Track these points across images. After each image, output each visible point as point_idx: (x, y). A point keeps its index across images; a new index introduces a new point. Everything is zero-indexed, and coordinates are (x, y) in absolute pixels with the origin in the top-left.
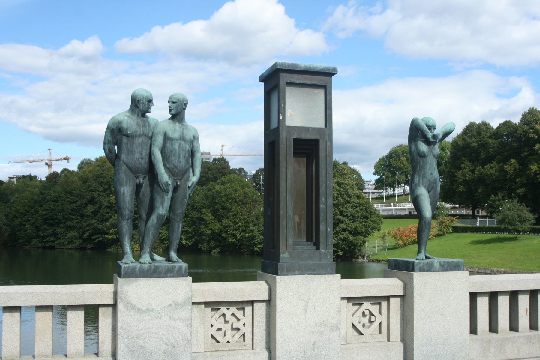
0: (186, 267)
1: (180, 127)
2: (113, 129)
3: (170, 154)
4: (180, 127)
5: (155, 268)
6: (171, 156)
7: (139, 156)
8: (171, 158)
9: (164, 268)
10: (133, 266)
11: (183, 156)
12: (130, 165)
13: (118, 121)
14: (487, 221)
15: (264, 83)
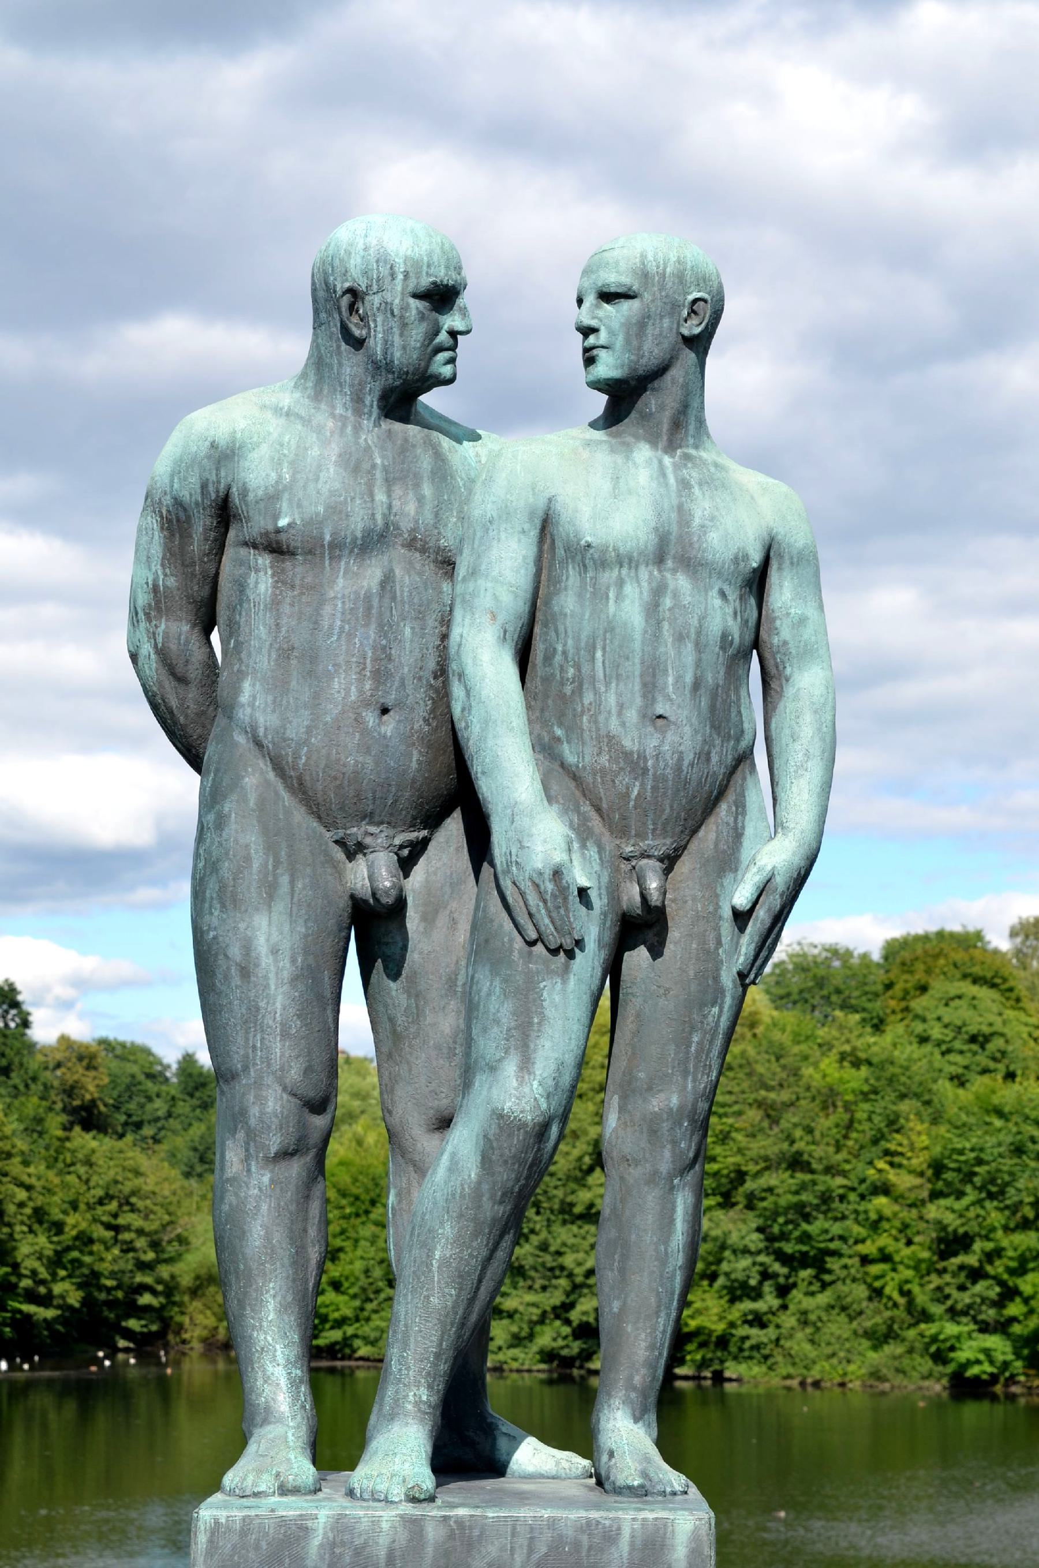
0: (695, 1537)
1: (663, 473)
3: (586, 669)
4: (663, 473)
6: (593, 679)
7: (361, 692)
8: (588, 698)
9: (522, 1541)
10: (283, 1521)
11: (679, 679)
13: (213, 445)
15: (606, 397)
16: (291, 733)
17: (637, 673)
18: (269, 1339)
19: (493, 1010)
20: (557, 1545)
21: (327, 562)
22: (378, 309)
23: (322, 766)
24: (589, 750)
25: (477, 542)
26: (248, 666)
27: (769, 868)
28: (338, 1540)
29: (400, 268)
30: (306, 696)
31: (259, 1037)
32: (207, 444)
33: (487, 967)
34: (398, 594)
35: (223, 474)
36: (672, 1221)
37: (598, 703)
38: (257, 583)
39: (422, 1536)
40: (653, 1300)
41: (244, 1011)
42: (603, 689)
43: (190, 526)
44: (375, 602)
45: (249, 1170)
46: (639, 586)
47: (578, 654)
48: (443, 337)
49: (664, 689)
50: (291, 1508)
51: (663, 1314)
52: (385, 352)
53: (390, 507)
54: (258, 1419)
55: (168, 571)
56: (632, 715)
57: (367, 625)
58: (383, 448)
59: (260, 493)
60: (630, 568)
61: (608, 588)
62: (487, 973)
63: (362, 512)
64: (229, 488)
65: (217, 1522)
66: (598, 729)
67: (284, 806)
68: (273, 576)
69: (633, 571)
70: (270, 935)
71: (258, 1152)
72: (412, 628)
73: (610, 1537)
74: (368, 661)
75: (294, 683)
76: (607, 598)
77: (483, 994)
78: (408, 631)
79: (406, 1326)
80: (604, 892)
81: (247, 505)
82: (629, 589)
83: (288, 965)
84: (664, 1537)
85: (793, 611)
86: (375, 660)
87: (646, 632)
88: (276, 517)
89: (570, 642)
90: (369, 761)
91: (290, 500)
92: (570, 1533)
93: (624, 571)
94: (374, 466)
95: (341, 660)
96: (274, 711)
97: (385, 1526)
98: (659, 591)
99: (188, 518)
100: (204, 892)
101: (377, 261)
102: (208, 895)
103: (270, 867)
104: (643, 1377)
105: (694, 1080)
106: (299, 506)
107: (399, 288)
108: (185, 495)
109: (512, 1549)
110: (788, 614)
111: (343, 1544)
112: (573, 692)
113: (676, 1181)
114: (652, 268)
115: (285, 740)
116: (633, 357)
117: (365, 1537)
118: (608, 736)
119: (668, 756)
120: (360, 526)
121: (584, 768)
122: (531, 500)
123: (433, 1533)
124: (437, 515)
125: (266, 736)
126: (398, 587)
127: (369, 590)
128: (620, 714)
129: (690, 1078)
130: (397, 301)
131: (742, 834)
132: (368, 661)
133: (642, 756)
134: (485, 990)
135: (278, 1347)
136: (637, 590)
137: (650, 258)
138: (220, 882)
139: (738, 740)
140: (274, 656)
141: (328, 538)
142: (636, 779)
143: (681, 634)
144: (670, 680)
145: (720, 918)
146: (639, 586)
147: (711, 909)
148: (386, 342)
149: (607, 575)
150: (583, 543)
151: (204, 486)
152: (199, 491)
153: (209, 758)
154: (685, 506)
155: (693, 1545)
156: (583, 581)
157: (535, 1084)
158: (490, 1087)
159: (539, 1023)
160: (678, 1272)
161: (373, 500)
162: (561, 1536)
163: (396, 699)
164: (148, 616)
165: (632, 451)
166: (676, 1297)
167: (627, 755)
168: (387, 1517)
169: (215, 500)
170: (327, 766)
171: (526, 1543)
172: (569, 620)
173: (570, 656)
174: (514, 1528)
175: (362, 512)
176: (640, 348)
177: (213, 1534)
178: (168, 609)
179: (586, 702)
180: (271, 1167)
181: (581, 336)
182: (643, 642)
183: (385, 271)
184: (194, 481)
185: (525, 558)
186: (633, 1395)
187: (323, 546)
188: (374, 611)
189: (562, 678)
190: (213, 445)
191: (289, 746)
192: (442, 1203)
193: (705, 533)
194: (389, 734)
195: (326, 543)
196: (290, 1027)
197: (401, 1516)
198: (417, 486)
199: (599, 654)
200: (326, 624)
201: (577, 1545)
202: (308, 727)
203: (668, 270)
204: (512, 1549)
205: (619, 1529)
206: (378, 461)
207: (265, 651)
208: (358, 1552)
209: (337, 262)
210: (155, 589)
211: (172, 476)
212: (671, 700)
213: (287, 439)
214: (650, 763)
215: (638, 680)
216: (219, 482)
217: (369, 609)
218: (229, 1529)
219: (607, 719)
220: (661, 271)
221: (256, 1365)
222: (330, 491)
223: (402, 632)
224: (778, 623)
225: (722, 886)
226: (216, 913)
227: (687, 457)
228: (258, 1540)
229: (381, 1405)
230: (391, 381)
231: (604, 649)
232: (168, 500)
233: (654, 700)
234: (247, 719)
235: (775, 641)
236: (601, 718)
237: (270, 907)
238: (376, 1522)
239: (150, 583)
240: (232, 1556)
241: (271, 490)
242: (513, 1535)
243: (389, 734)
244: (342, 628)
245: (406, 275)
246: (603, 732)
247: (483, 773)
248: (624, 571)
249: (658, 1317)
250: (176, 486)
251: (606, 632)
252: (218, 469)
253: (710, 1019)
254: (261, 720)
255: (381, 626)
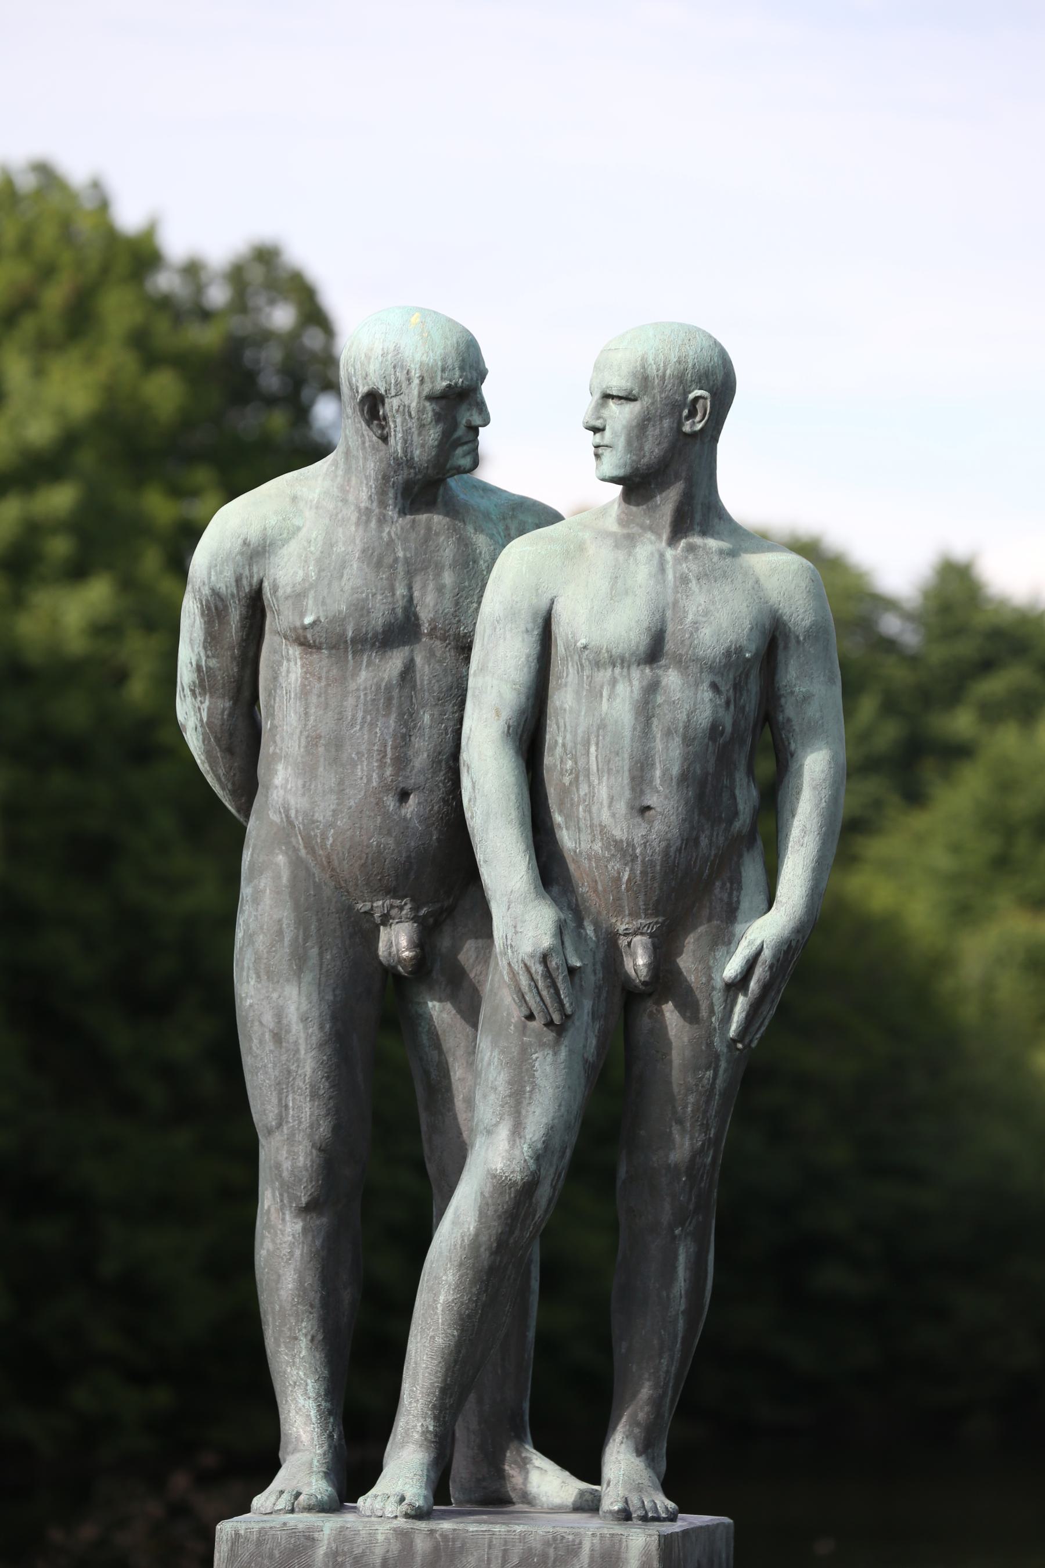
0: (646, 1552)
1: (662, 569)
2: (215, 593)
3: (581, 763)
4: (662, 569)
5: (436, 1549)
6: (588, 771)
7: (381, 777)
8: (584, 789)
9: (497, 1553)
10: (293, 1533)
11: (664, 773)
12: (324, 838)
13: (246, 543)
14: (450, 1504)
15: (621, 486)
16: (318, 816)
17: (626, 768)
18: (301, 1373)
19: (491, 1078)
20: (528, 1555)
21: (350, 657)
22: (397, 411)
23: (347, 846)
24: (585, 837)
25: (486, 639)
26: (281, 749)
27: (758, 942)
28: (340, 1549)
29: (415, 375)
30: (332, 781)
31: (290, 1097)
32: (240, 541)
33: (490, 1038)
34: (418, 683)
35: (255, 569)
36: (674, 1268)
37: (591, 794)
38: (288, 672)
39: (411, 1547)
40: (655, 1342)
41: (277, 1074)
42: (596, 782)
43: (227, 614)
44: (395, 693)
45: (283, 1220)
46: (631, 685)
47: (575, 747)
48: (461, 431)
49: (651, 782)
50: (303, 1520)
51: (666, 1355)
52: (405, 452)
53: (411, 599)
54: (290, 1448)
55: (209, 653)
56: (621, 807)
57: (387, 715)
58: (405, 540)
59: (289, 590)
60: (622, 668)
61: (602, 687)
62: (489, 1044)
63: (383, 607)
64: (261, 582)
65: (237, 1534)
66: (591, 819)
67: (315, 882)
68: (302, 666)
69: (625, 670)
70: (300, 1003)
71: (290, 1202)
72: (432, 715)
73: (573, 1550)
74: (389, 749)
75: (321, 769)
76: (601, 695)
77: (485, 1063)
78: (427, 718)
79: (416, 1363)
80: (599, 967)
81: (277, 600)
82: (622, 688)
83: (317, 1032)
84: (619, 1552)
85: (797, 689)
86: (394, 748)
87: (634, 729)
88: (302, 615)
89: (569, 736)
90: (391, 841)
91: (315, 598)
92: (538, 1546)
93: (617, 670)
94: (396, 560)
95: (363, 748)
96: (303, 795)
97: (380, 1538)
98: (652, 688)
99: (226, 607)
100: (243, 961)
101: (394, 367)
102: (245, 965)
103: (300, 940)
104: (648, 1414)
105: (691, 1139)
106: (324, 603)
107: (416, 392)
108: (221, 587)
109: (489, 1560)
110: (792, 693)
111: (344, 1554)
112: (571, 783)
113: (677, 1232)
114: (652, 371)
115: (313, 822)
116: (634, 458)
117: (364, 1547)
118: (600, 825)
119: (655, 844)
120: (380, 622)
121: (581, 853)
122: (534, 601)
123: (421, 1545)
124: (457, 603)
125: (297, 817)
126: (418, 676)
127: (390, 681)
128: (610, 806)
129: (688, 1137)
130: (414, 405)
131: (737, 909)
132: (389, 749)
133: (631, 844)
134: (486, 1059)
135: (309, 1381)
136: (629, 689)
137: (651, 361)
138: (256, 954)
139: (730, 822)
140: (303, 743)
141: (350, 634)
142: (626, 864)
143: (669, 729)
144: (658, 773)
145: (713, 988)
146: (631, 685)
147: (704, 980)
148: (405, 441)
149: (601, 673)
150: (579, 644)
151: (238, 580)
152: (234, 584)
153: (250, 833)
154: (681, 604)
155: (644, 1559)
156: (581, 678)
157: (525, 1147)
158: (487, 1149)
159: (530, 1092)
160: (680, 1317)
161: (394, 595)
162: (530, 1549)
163: (415, 784)
164: (193, 692)
165: (634, 546)
166: (679, 1340)
167: (617, 843)
168: (383, 1531)
169: (250, 592)
170: (351, 847)
171: (500, 1554)
172: (567, 714)
173: (569, 749)
174: (491, 1541)
175: (383, 607)
176: (641, 448)
177: (233, 1544)
178: (211, 687)
179: (582, 793)
180: (303, 1215)
181: (592, 433)
182: (632, 740)
183: (401, 376)
184: (229, 574)
185: (528, 656)
186: (637, 1430)
187: (346, 641)
188: (395, 702)
189: (562, 769)
190: (246, 543)
191: (318, 827)
192: (446, 1253)
193: (697, 629)
194: (409, 816)
195: (349, 638)
196: (319, 1088)
197: (395, 1530)
198: (438, 575)
199: (593, 749)
200: (349, 715)
201: (544, 1556)
202: (334, 811)
203: (668, 372)
204: (489, 1560)
205: (580, 1543)
206: (401, 554)
207: (296, 737)
208: (357, 1560)
209: (358, 366)
210: (199, 668)
211: (210, 568)
212: (658, 792)
213: (314, 536)
214: (638, 851)
215: (627, 774)
216: (252, 577)
217: (389, 700)
218: (247, 1539)
219: (600, 810)
220: (660, 373)
221: (289, 1398)
222: (352, 589)
223: (422, 718)
224: (783, 700)
225: (715, 958)
226: (252, 982)
227: (691, 548)
228: (272, 1550)
229: (395, 1435)
230: (412, 475)
231: (597, 744)
232: (206, 591)
233: (642, 792)
234: (280, 801)
235: (781, 718)
236: (594, 809)
237: (299, 978)
238: (372, 1535)
239: (194, 663)
240: (250, 1563)
241: (298, 588)
242: (490, 1547)
243: (409, 816)
244: (364, 718)
245: (422, 381)
246: (596, 822)
247: (485, 862)
248: (617, 670)
249: (661, 1357)
250: (213, 578)
251: (599, 729)
252: (250, 565)
253: (705, 1081)
254: (292, 802)
255: (401, 715)
